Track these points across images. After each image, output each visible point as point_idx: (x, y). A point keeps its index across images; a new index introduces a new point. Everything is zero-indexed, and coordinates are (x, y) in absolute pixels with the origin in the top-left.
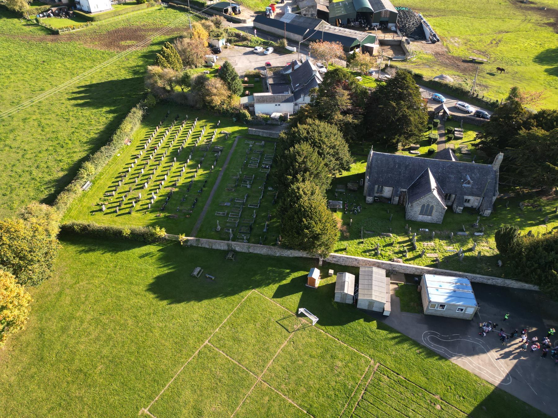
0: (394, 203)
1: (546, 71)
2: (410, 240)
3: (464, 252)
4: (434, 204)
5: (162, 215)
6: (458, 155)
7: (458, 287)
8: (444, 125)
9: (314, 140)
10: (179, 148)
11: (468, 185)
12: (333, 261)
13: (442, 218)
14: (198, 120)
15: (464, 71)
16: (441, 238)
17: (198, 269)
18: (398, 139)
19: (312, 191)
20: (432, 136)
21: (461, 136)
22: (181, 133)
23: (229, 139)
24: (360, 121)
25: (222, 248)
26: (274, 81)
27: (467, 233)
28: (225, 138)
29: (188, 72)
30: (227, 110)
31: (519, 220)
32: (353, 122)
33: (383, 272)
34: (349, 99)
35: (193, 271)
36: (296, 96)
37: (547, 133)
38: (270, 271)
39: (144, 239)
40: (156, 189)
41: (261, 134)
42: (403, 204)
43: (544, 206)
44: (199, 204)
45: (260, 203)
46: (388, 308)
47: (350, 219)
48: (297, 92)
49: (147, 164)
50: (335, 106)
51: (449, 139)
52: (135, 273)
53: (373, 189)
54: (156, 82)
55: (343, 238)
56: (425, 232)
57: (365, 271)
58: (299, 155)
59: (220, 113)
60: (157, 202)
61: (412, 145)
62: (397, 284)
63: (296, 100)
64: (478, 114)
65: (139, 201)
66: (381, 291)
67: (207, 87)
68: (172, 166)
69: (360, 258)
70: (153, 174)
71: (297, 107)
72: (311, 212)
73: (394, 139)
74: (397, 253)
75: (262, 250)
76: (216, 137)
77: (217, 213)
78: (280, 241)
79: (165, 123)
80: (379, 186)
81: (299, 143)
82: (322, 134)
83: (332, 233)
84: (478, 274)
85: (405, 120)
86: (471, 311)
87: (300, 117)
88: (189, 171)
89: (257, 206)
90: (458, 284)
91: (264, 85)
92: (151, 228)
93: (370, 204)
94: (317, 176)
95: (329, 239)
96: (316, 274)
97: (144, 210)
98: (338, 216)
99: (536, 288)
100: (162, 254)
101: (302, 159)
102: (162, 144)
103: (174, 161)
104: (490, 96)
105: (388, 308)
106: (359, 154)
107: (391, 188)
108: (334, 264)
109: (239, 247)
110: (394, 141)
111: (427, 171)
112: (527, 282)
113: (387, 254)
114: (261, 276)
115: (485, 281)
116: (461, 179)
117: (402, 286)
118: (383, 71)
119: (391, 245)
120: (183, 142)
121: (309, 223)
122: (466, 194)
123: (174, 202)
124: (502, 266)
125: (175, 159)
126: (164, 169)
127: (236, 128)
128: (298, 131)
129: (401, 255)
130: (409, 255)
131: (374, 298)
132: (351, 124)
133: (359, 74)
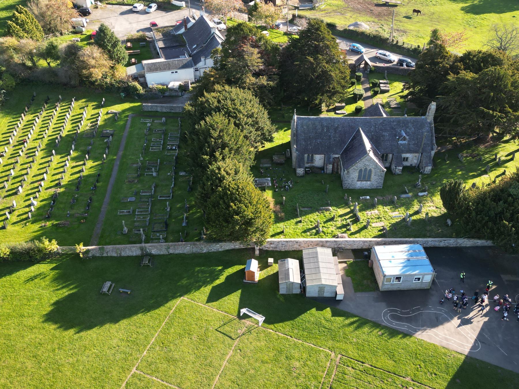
0: (328, 172)
1: (463, 9)
2: (352, 211)
4: (371, 167)
5: (49, 224)
6: (387, 109)
9: (228, 109)
10: (57, 138)
11: (404, 142)
12: (271, 248)
13: (382, 181)
14: (75, 100)
15: (379, 16)
16: (384, 204)
17: (108, 284)
18: (321, 100)
19: (235, 169)
20: (357, 92)
21: (387, 89)
22: (55, 118)
23: (120, 119)
26: (165, 44)
27: (410, 194)
28: (114, 118)
30: (112, 84)
31: (460, 173)
32: (268, 84)
33: (329, 251)
35: (101, 288)
36: (195, 60)
37: (477, 76)
38: (198, 272)
39: (30, 257)
40: (35, 193)
41: (159, 109)
42: (337, 172)
43: (483, 155)
44: (95, 204)
45: (173, 192)
46: (340, 291)
47: (282, 196)
48: (195, 54)
49: (17, 162)
50: (244, 67)
51: (376, 93)
52: (25, 302)
54: (12, 57)
55: (278, 220)
56: (366, 200)
57: (309, 254)
58: (213, 129)
59: (102, 89)
60: (38, 209)
61: (337, 104)
62: (345, 262)
63: (195, 65)
64: (401, 62)
65: (13, 211)
66: (329, 274)
67: (81, 59)
68: (51, 161)
69: (301, 239)
71: (198, 73)
72: (238, 195)
73: (316, 100)
74: (340, 228)
75: (185, 248)
76: (103, 119)
77: (120, 212)
78: (205, 235)
79: (33, 108)
80: (309, 156)
82: (236, 101)
83: (266, 215)
84: (429, 237)
85: (325, 77)
87: (204, 84)
89: (169, 197)
90: (411, 251)
91: (152, 49)
92: (37, 242)
93: (301, 177)
94: (237, 151)
95: (263, 223)
96: (254, 265)
97: (24, 221)
98: (268, 195)
99: (489, 243)
100: (57, 273)
101: (218, 133)
102: (33, 134)
103: (53, 155)
104: (410, 41)
105: (340, 291)
106: (281, 121)
108: (272, 251)
109: (155, 249)
111: (359, 129)
112: (479, 238)
113: (329, 231)
114: (188, 279)
115: (437, 244)
116: (396, 136)
118: (292, 22)
119: (332, 219)
123: (62, 206)
124: (452, 225)
125: (54, 152)
126: (42, 166)
127: (127, 106)
128: (207, 101)
129: (345, 229)
130: (354, 228)
131: (324, 282)
132: (265, 87)
133: (264, 28)
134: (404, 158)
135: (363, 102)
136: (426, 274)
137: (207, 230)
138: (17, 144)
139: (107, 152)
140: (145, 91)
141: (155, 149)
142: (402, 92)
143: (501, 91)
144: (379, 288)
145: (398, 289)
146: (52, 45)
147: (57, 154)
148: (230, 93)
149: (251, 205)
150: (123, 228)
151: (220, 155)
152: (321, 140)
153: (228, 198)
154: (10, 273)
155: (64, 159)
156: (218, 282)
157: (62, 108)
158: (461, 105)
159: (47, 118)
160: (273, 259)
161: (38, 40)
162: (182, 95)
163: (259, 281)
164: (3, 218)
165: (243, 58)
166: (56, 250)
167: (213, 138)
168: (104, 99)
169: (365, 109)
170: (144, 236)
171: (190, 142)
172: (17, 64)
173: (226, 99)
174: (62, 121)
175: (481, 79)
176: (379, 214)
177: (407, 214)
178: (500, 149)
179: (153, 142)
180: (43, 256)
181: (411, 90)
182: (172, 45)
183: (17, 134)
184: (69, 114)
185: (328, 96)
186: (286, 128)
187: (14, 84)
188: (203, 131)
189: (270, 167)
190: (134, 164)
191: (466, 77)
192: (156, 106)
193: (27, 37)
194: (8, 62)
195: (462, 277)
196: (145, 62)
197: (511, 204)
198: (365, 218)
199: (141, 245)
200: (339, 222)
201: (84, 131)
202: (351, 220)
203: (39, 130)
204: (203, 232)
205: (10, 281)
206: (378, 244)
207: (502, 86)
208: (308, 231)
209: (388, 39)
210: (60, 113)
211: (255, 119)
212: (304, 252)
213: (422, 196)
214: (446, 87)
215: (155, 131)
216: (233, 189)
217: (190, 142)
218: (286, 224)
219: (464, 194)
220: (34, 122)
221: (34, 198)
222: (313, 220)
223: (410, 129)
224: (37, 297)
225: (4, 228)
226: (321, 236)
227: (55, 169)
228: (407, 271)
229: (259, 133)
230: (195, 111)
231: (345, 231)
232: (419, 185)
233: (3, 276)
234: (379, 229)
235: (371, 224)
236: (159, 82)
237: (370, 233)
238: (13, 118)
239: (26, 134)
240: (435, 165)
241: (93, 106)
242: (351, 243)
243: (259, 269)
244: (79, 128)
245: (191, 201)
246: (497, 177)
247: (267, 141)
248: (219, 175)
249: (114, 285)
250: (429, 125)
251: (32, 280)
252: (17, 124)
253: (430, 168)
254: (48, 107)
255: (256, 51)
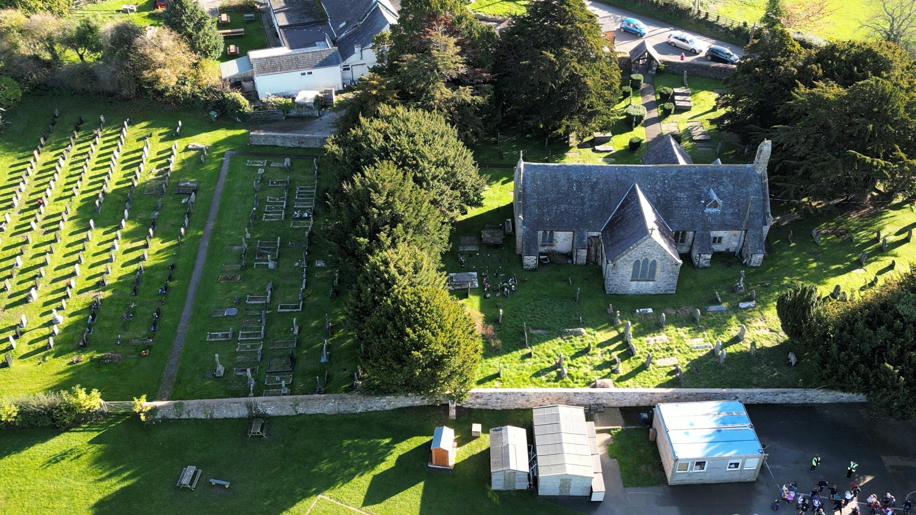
0: (579, 262)
2: (621, 337)
3: (725, 345)
4: (656, 257)
5: (85, 358)
6: (687, 144)
7: (724, 422)
8: (652, 83)
9: (402, 152)
10: (97, 196)
11: (715, 210)
12: (477, 404)
13: (675, 282)
14: (129, 124)
16: (679, 323)
17: (190, 470)
18: (568, 126)
19: (415, 264)
20: (632, 111)
21: (687, 104)
22: (94, 158)
23: (210, 160)
24: (487, 96)
25: (236, 415)
26: (289, 19)
27: (725, 305)
28: (199, 158)
29: (92, 19)
30: (194, 96)
31: (814, 265)
32: (473, 101)
33: (580, 412)
34: (458, 54)
35: (179, 477)
36: (344, 50)
37: (844, 92)
38: (348, 448)
39: (53, 420)
40: (59, 300)
41: (279, 143)
42: (596, 263)
43: (855, 231)
44: (166, 321)
45: (304, 299)
46: (599, 487)
47: (498, 307)
48: (343, 39)
49: (26, 242)
50: (432, 71)
51: (666, 113)
52: (45, 502)
53: (536, 239)
54: (15, 46)
55: (490, 352)
56: (647, 314)
57: (544, 417)
58: (376, 192)
59: (177, 103)
60: (66, 330)
61: (598, 135)
62: (608, 431)
63: (344, 60)
64: (714, 55)
65: (22, 333)
67: (141, 51)
68: (87, 239)
69: (530, 389)
70: (45, 264)
71: (348, 74)
72: (420, 313)
73: (560, 127)
74: (599, 368)
75: (325, 405)
76: (179, 160)
77: (211, 337)
78: (360, 379)
79: (53, 139)
80: (545, 232)
81: (372, 162)
82: (417, 136)
83: (468, 348)
84: (757, 386)
86: (752, 464)
87: (362, 103)
88: (129, 246)
89: (297, 307)
90: (723, 414)
91: (267, 27)
92: (64, 393)
93: (532, 270)
94: (419, 229)
95: (464, 362)
96: (447, 438)
97: (41, 351)
98: (472, 306)
99: (860, 398)
100: (100, 450)
101: (384, 198)
102: (56, 189)
103: (89, 228)
105: (599, 487)
106: (495, 166)
107: (569, 234)
108: (480, 410)
109: (273, 406)
110: (561, 131)
111: (634, 187)
112: (843, 390)
113: (581, 374)
114: (330, 461)
115: (770, 399)
116: (700, 198)
117: (619, 433)
119: (586, 351)
120: (103, 181)
121: (419, 336)
122: (713, 228)
123: (107, 324)
124: (796, 364)
125: (92, 222)
126: (70, 250)
127: (221, 134)
128: (366, 134)
129: (609, 370)
130: (624, 368)
131: (570, 471)
132: (469, 105)
134: (715, 238)
135: (643, 128)
136: (749, 457)
137: (364, 371)
138: (27, 207)
139: (186, 222)
140: (255, 108)
141: (271, 217)
142: (714, 109)
143: (887, 120)
144: (666, 480)
145: (700, 482)
146: (89, 27)
147: (97, 226)
148: (406, 120)
149: (442, 331)
150: (215, 366)
151: (388, 236)
152: (567, 207)
153: (401, 319)
154: (18, 448)
155: (110, 236)
156: (382, 467)
157: (106, 139)
158: (816, 142)
159: (79, 158)
160: (480, 425)
161: (61, 14)
162: (320, 116)
163: (456, 465)
164: (4, 346)
165: (430, 54)
166: (98, 407)
167: (374, 206)
168: (180, 123)
169: (648, 143)
170: (253, 381)
171: (334, 212)
172: (24, 59)
173: (399, 134)
174: (106, 164)
175: (852, 98)
176: (669, 342)
177: (718, 342)
178: (886, 221)
179: (268, 203)
180: (76, 419)
181: (729, 109)
182: (302, 21)
183: (27, 188)
184: (118, 151)
185: (580, 121)
186: (505, 179)
187: (20, 94)
188: (357, 194)
189: (476, 252)
190: (234, 245)
191: (826, 95)
192: (274, 137)
193: (41, 8)
194: (9, 54)
195: (814, 464)
196: (254, 54)
197: (899, 333)
198: (644, 350)
199: (247, 399)
200: (598, 357)
201: (145, 183)
202: (619, 352)
203: (65, 181)
204: (358, 374)
205: (18, 464)
206: (667, 399)
207: (889, 113)
208: (543, 374)
209: (690, 9)
210: (102, 149)
211: (449, 169)
212: (536, 413)
213: (745, 309)
214: (790, 109)
215: (272, 183)
216: (411, 302)
217: (334, 212)
218: (504, 360)
219: (818, 312)
220: (56, 164)
221: (58, 309)
222: (552, 353)
223: (725, 187)
224: (66, 493)
225: (5, 365)
226: (565, 382)
227: (95, 255)
228: (717, 450)
229: (458, 193)
230: (345, 155)
231: (609, 374)
232: (741, 288)
233: (5, 455)
234: (669, 370)
235: (654, 360)
236: (279, 92)
237: (651, 377)
238: (19, 158)
239: (42, 188)
240: (769, 248)
241: (160, 135)
242: (618, 397)
243: (456, 444)
244: (136, 178)
245: (336, 315)
246: (880, 273)
247: (471, 205)
248: (386, 276)
249: (200, 471)
250: (759, 180)
251: (57, 461)
252: (25, 169)
253: (761, 256)
254: (80, 137)
255: (453, 40)
